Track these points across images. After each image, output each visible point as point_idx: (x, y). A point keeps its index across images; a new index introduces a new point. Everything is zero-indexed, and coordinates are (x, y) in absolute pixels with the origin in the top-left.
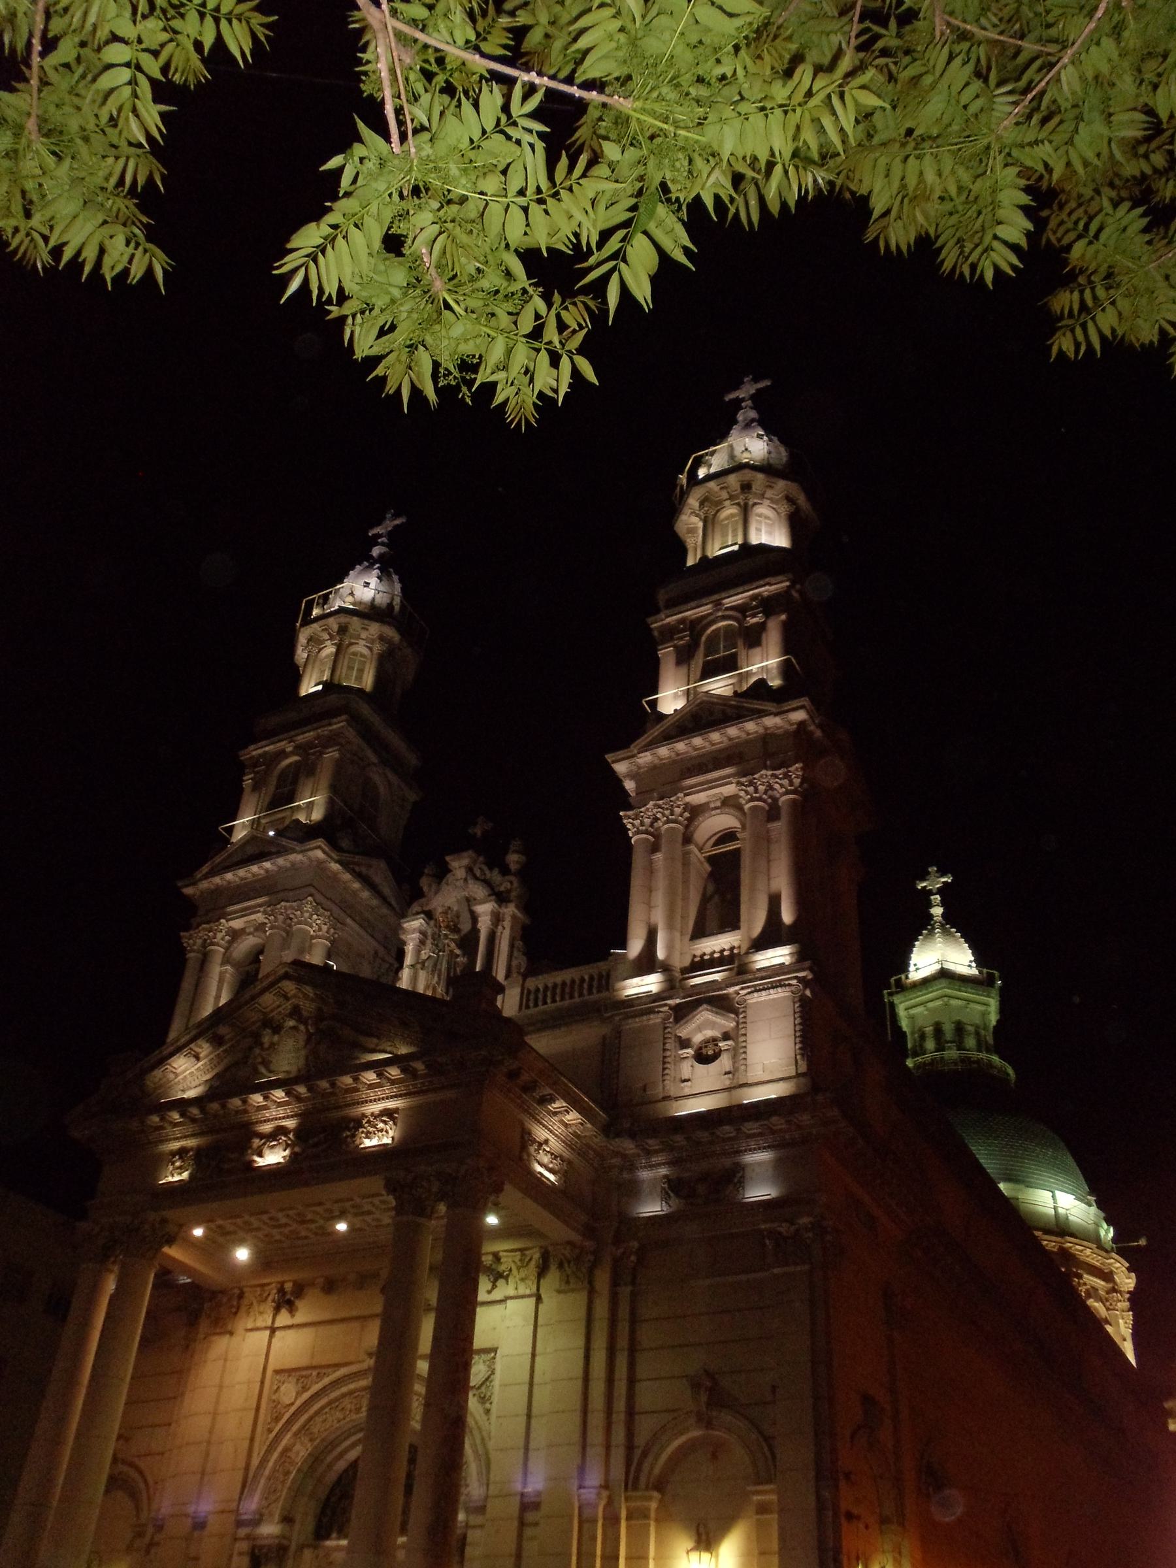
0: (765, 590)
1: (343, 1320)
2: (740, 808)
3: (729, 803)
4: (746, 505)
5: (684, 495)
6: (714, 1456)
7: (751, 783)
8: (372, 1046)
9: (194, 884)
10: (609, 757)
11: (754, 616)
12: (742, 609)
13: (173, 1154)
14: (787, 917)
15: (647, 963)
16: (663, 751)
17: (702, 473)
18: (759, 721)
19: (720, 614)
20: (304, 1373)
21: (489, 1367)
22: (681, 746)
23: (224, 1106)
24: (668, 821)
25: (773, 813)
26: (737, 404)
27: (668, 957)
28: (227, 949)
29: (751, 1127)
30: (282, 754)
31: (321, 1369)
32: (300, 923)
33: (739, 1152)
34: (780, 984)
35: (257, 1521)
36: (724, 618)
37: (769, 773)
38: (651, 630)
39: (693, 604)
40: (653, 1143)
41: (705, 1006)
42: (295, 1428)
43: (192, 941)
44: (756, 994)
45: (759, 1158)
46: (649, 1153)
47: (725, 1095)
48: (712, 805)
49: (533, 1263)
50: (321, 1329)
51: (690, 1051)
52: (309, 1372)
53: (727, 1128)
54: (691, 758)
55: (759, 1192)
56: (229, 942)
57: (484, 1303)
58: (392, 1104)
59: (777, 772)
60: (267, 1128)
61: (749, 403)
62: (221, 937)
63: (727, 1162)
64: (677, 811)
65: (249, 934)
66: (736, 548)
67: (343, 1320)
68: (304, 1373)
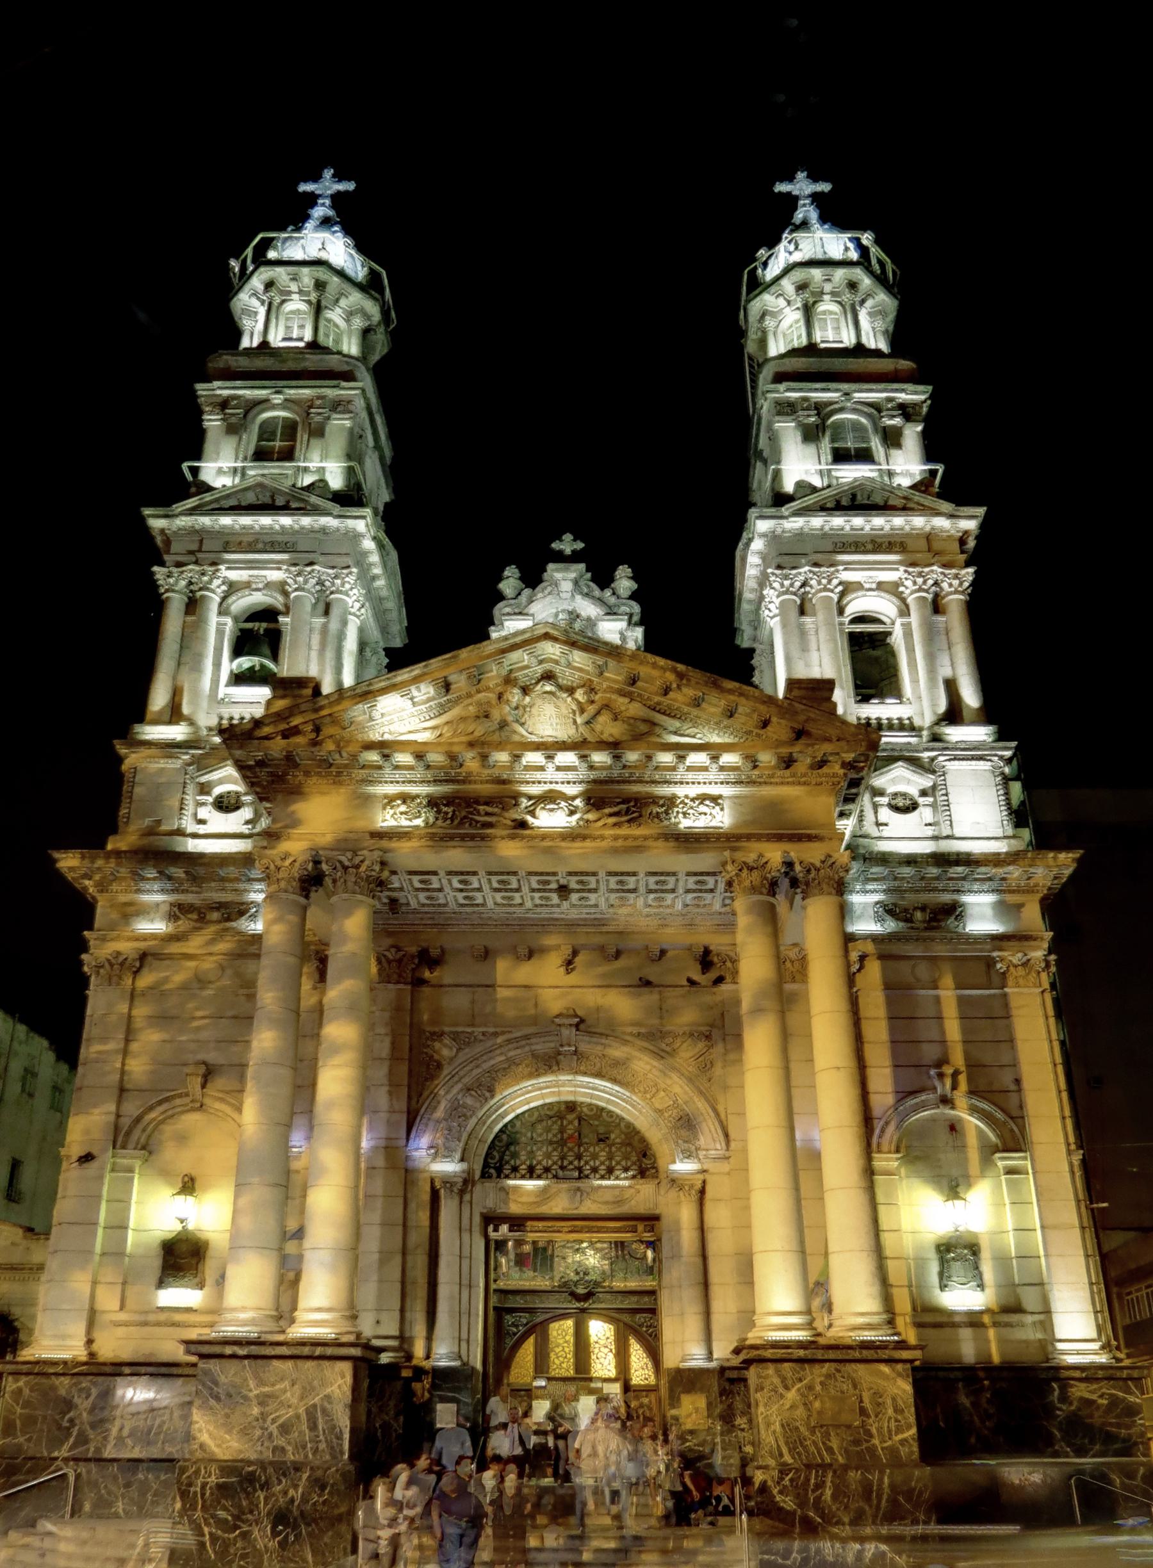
0: (902, 397)
2: (286, 594)
3: (892, 589)
4: (319, 302)
5: (245, 276)
7: (920, 575)
10: (147, 511)
14: (971, 697)
15: (174, 714)
17: (272, 255)
18: (296, 518)
26: (312, 200)
27: (845, 712)
28: (224, 599)
30: (262, 403)
37: (940, 570)
38: (197, 397)
40: (876, 870)
41: (900, 763)
43: (172, 582)
44: (956, 762)
46: (868, 880)
48: (867, 586)
51: (210, 799)
53: (960, 869)
56: (224, 592)
58: (714, 790)
59: (947, 572)
61: (328, 202)
62: (217, 588)
63: (947, 898)
64: (835, 582)
66: (301, 344)
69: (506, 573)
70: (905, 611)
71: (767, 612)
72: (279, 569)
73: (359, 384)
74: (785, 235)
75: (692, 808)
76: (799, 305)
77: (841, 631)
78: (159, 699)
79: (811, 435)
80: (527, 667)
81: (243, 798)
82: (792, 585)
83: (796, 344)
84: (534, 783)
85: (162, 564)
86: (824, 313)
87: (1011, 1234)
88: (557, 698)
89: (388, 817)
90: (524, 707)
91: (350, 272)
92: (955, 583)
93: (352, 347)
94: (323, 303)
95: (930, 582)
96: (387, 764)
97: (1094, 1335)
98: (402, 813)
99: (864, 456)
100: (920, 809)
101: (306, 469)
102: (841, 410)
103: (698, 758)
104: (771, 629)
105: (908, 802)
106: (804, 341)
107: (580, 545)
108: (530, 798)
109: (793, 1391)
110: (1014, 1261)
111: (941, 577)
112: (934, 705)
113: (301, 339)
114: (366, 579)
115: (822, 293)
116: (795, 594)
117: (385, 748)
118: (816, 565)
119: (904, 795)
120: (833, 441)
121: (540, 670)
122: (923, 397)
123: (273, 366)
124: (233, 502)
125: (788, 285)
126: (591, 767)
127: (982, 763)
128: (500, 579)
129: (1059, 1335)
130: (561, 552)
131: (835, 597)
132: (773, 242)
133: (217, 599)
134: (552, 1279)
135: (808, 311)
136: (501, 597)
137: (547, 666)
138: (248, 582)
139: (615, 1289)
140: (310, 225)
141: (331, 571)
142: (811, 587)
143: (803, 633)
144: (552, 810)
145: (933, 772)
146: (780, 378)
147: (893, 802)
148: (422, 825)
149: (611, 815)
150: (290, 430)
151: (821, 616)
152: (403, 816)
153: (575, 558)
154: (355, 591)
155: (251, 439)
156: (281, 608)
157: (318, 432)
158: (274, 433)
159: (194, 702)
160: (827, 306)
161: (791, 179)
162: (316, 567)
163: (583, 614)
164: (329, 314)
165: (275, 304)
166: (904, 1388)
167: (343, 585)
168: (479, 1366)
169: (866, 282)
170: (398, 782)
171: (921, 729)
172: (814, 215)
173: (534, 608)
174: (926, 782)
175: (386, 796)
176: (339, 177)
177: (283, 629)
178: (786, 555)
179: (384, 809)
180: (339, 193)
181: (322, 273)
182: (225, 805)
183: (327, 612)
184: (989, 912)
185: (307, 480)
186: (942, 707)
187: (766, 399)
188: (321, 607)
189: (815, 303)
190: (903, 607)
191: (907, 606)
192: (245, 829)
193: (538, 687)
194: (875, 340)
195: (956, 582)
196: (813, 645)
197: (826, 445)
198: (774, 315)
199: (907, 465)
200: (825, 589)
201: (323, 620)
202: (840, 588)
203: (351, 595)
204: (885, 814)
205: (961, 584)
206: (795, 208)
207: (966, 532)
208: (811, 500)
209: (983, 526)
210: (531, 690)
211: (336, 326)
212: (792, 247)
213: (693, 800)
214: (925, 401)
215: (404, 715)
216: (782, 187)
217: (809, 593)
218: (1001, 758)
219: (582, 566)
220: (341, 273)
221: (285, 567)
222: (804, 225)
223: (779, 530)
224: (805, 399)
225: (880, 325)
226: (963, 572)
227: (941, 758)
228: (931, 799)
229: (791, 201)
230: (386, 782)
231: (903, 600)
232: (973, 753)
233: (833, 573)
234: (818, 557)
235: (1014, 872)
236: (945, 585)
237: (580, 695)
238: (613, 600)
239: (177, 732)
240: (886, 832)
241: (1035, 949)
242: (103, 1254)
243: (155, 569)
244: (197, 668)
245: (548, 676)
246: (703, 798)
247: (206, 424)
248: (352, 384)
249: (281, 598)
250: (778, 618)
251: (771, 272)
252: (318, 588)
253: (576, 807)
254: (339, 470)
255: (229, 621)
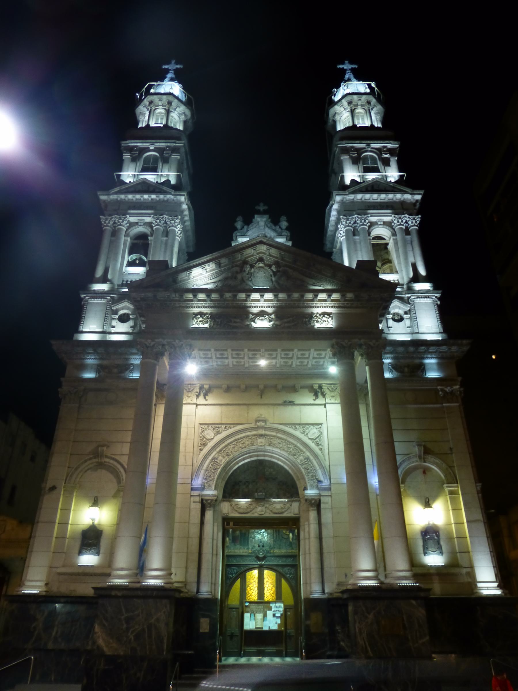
0: (390, 146)
1: (228, 404)
2: (152, 227)
3: (388, 224)
4: (169, 110)
6: (424, 472)
8: (312, 283)
9: (108, 195)
10: (99, 193)
11: (386, 154)
12: (379, 151)
13: (196, 315)
14: (422, 271)
15: (104, 280)
16: (359, 196)
17: (152, 91)
19: (369, 149)
20: (218, 426)
21: (320, 431)
22: (367, 196)
23: (235, 296)
24: (158, 225)
25: (407, 231)
26: (167, 71)
28: (127, 230)
29: (432, 349)
30: (147, 150)
31: (228, 425)
32: (170, 227)
33: (424, 358)
34: (428, 297)
35: (203, 488)
36: (371, 151)
37: (408, 216)
39: (358, 142)
42: (218, 450)
43: (107, 222)
44: (419, 299)
45: (90, 361)
47: (410, 335)
48: (379, 223)
49: (337, 390)
50: (224, 407)
51: (117, 316)
52: (220, 426)
53: (423, 348)
54: (370, 202)
55: (433, 374)
56: (128, 226)
57: (185, 404)
58: (329, 310)
59: (411, 217)
60: (255, 310)
61: (173, 72)
63: (417, 361)
64: (367, 221)
65: (141, 225)
66: (162, 126)
67: (228, 404)
68: (218, 426)
69: (238, 219)
70: (394, 234)
71: (339, 235)
72: (150, 217)
73: (183, 142)
74: (342, 84)
75: (320, 318)
76: (349, 110)
77: (370, 243)
78: (99, 273)
79: (355, 161)
80: (253, 255)
81: (131, 316)
82: (350, 223)
83: (347, 125)
84: (255, 307)
85: (104, 215)
86: (358, 113)
87: (453, 525)
88: (265, 269)
89: (194, 323)
90: (251, 273)
91: (180, 97)
92: (413, 222)
93: (180, 127)
94: (171, 110)
95: (404, 221)
96: (195, 299)
97: (494, 579)
98: (200, 321)
99: (376, 170)
100: (405, 320)
101: (161, 175)
102: (366, 151)
103: (322, 296)
104: (341, 243)
105: (399, 318)
106: (351, 124)
107: (266, 208)
108: (253, 314)
109: (372, 614)
110: (456, 539)
111: (408, 219)
112: (408, 273)
113: (162, 124)
114: (183, 222)
115: (358, 105)
116: (351, 227)
117: (196, 291)
118: (358, 215)
119: (398, 314)
120: (363, 164)
121: (257, 257)
122: (398, 146)
123: (150, 133)
124: (132, 189)
125: (345, 102)
126: (278, 301)
127: (429, 299)
128: (235, 221)
129: (479, 579)
130: (259, 210)
131: (367, 228)
132: (338, 87)
133: (125, 229)
134: (248, 549)
135: (352, 112)
136: (236, 229)
137: (261, 255)
138: (138, 222)
139: (276, 554)
140: (166, 80)
141: (170, 218)
142: (358, 224)
143: (355, 243)
144: (262, 320)
145: (409, 303)
146: (342, 139)
147: (394, 318)
148: (208, 327)
149: (286, 323)
150: (155, 159)
151: (362, 235)
152: (201, 323)
153: (264, 213)
154: (179, 226)
155: (140, 164)
156: (149, 233)
157: (166, 161)
158: (149, 161)
159: (113, 274)
160: (359, 110)
161: (343, 63)
162: (165, 216)
163: (268, 235)
164: (172, 114)
165: (153, 110)
166: (421, 613)
167: (175, 223)
168: (219, 598)
169: (373, 101)
170: (199, 307)
171: (403, 285)
172: (352, 77)
173: (249, 233)
174: (407, 308)
175: (194, 314)
176: (177, 63)
177: (150, 242)
178: (347, 210)
179: (193, 319)
180: (177, 68)
181: (171, 98)
182: (123, 319)
183: (167, 236)
184: (435, 367)
185: (163, 180)
186: (411, 275)
187: (337, 147)
188: (165, 233)
189: (355, 109)
190: (394, 232)
191: (395, 232)
192: (130, 330)
193: (257, 264)
194: (378, 124)
195: (414, 221)
196: (359, 249)
197: (361, 165)
198: (339, 114)
199: (393, 174)
200: (363, 225)
201: (165, 238)
202: (369, 224)
203: (178, 229)
204: (391, 323)
205: (416, 222)
206: (345, 74)
207: (417, 201)
208: (357, 187)
209: (422, 198)
210: (254, 266)
211: (175, 119)
212: (345, 88)
213: (320, 315)
214: (398, 147)
215: (202, 276)
216: (341, 66)
217: (356, 226)
218: (436, 297)
219: (267, 216)
220: (177, 98)
221: (152, 216)
222: (349, 80)
223: (345, 200)
224: (353, 147)
225: (379, 117)
226: (417, 217)
227: (412, 297)
228: (409, 316)
229: (344, 71)
230: (194, 307)
231: (394, 229)
232: (424, 293)
233: (366, 218)
234: (359, 211)
235: (444, 348)
236: (410, 223)
237: (274, 268)
238: (280, 230)
239: (104, 287)
240: (392, 330)
241: (456, 385)
242: (56, 538)
243: (101, 217)
244: (116, 260)
245: (261, 260)
246: (324, 314)
247: (124, 157)
248: (180, 142)
249: (150, 229)
250: (344, 237)
251: (336, 99)
252: (165, 225)
253: (272, 318)
254: (174, 176)
255: (129, 238)
